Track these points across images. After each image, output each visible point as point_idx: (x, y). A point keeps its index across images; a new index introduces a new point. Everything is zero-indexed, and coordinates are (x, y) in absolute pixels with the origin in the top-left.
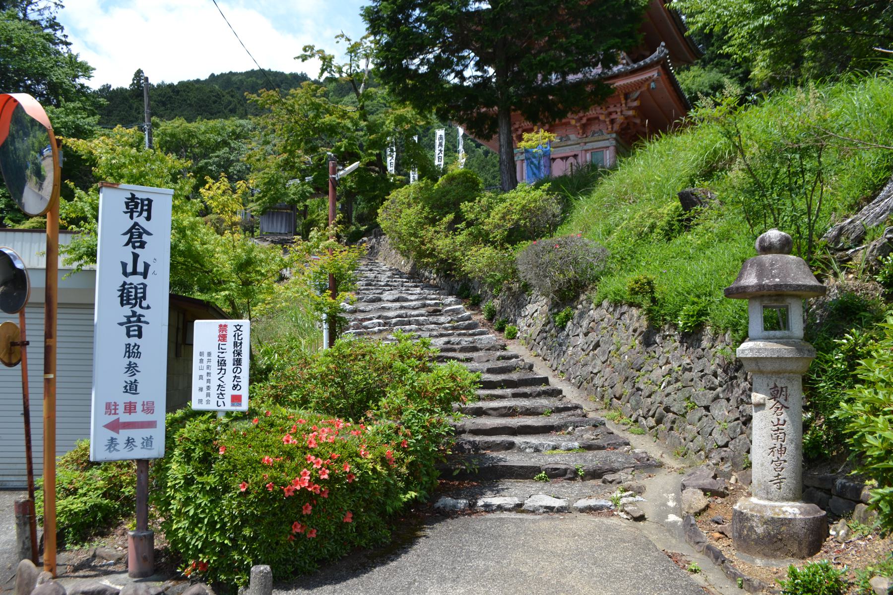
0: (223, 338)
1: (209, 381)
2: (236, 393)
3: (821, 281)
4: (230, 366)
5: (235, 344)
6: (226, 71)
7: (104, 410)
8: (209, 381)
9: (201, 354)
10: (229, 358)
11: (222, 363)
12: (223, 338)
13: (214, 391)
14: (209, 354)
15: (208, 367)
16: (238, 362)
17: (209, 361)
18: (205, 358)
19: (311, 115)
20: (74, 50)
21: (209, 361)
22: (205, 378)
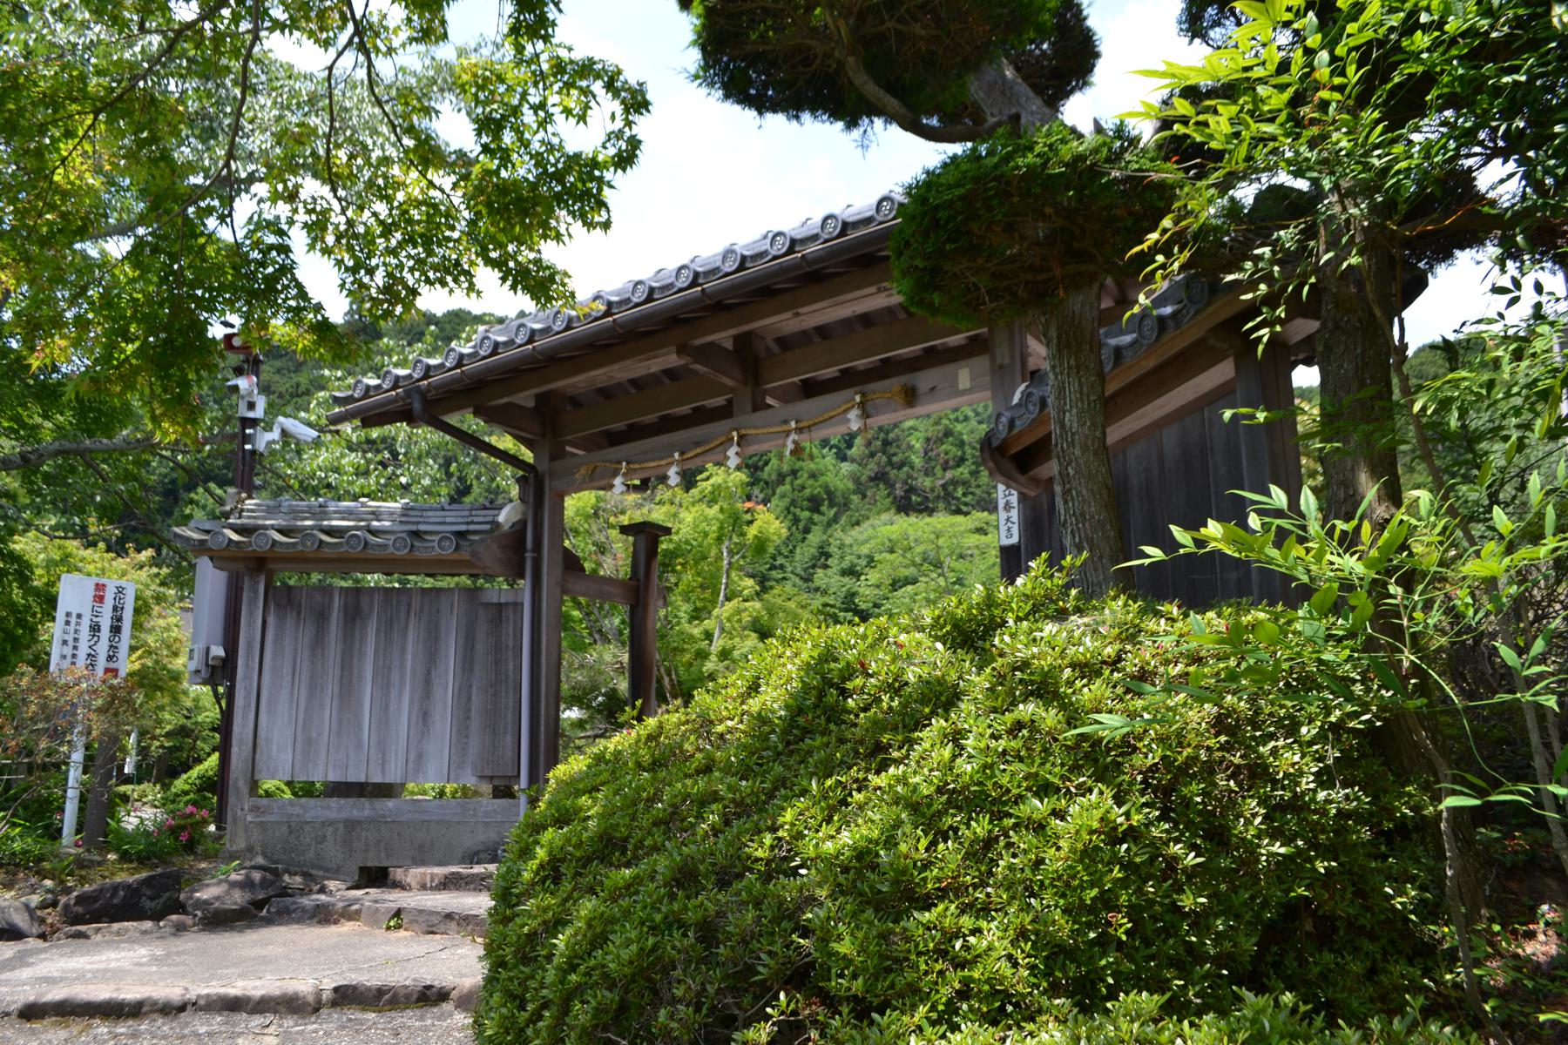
0: (100, 599)
1: (75, 648)
2: (112, 665)
3: (135, 371)
4: (105, 632)
5: (115, 609)
6: (776, 121)
7: (371, 863)
8: (75, 648)
9: (68, 614)
10: (106, 623)
11: (95, 629)
12: (100, 599)
13: (82, 660)
14: (79, 616)
15: (76, 631)
16: (116, 630)
17: (78, 624)
18: (73, 620)
19: (995, 202)
20: (571, 149)
21: (78, 624)
22: (71, 643)
